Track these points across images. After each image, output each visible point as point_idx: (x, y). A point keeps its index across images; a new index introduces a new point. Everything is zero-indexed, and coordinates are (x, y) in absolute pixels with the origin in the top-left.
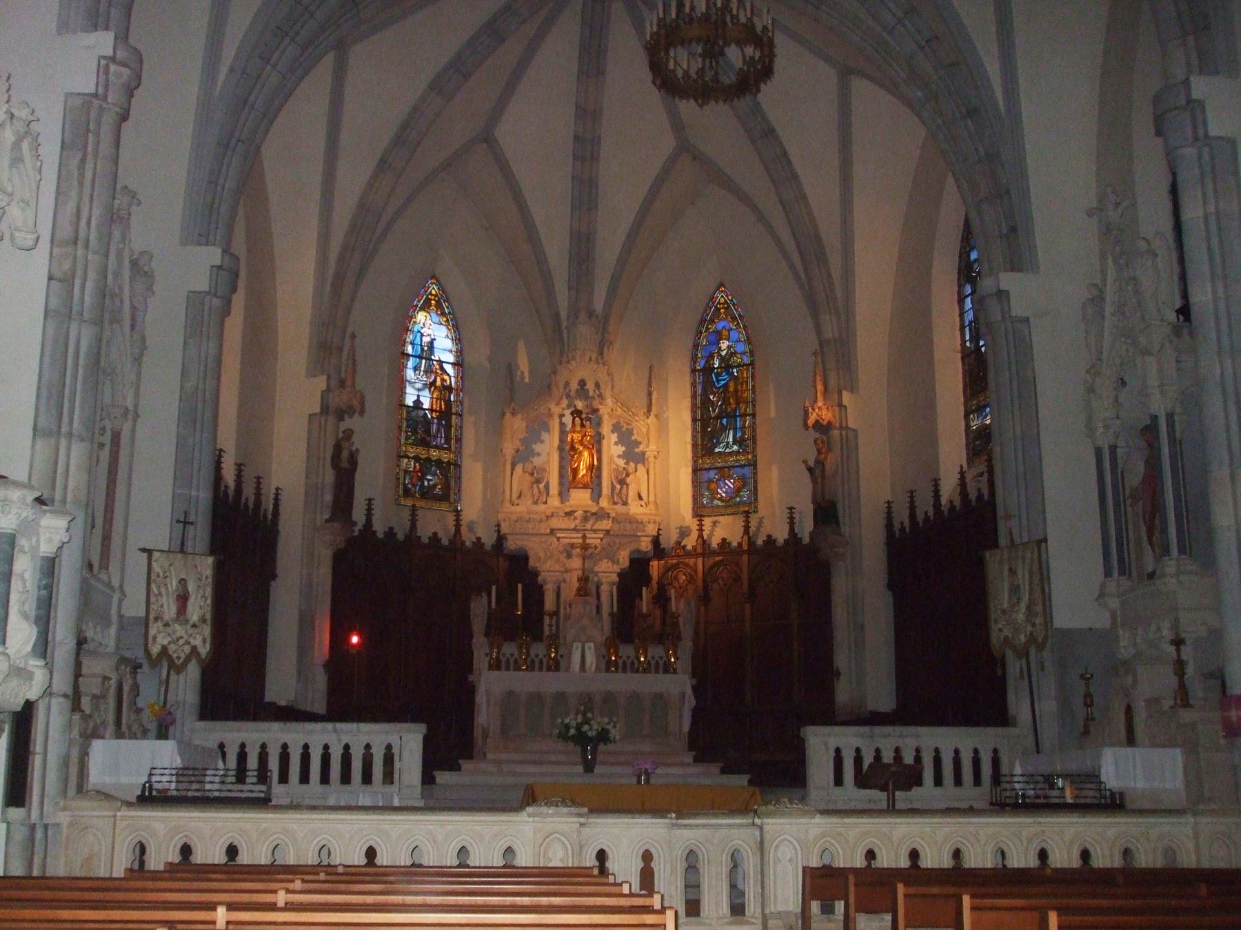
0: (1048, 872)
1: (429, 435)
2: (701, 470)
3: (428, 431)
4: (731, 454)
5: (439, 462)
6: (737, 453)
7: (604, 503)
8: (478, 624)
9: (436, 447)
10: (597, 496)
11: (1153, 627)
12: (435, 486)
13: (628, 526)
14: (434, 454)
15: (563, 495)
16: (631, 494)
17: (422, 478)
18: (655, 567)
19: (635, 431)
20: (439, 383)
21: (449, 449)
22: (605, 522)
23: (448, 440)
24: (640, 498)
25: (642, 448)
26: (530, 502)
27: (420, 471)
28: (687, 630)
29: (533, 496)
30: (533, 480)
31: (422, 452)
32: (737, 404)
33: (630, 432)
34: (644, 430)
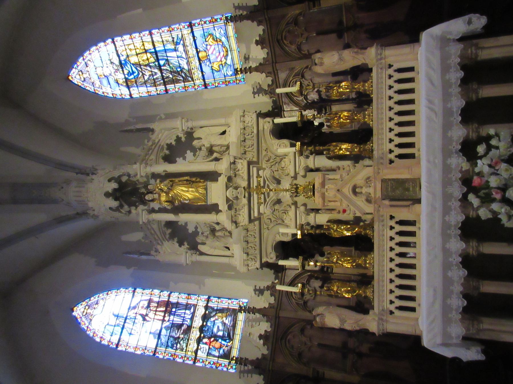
0: (301, 258)
1: (182, 325)
2: (139, 54)
3: (179, 326)
4: (186, 52)
5: (205, 318)
6: (184, 45)
7: (222, 167)
8: (352, 321)
9: (192, 319)
10: (211, 176)
11: (362, 149)
12: (224, 324)
13: (248, 143)
14: (198, 322)
15: (214, 209)
16: (219, 142)
17: (216, 337)
18: (291, 116)
19: (169, 142)
20: (144, 312)
21: (195, 306)
22: (239, 166)
23: (187, 307)
24: (224, 133)
25: (181, 135)
26: (231, 240)
27: (209, 338)
28: (350, 59)
29: (225, 236)
30: (211, 237)
31: (195, 334)
32: (146, 51)
33: (169, 146)
34: (166, 133)
